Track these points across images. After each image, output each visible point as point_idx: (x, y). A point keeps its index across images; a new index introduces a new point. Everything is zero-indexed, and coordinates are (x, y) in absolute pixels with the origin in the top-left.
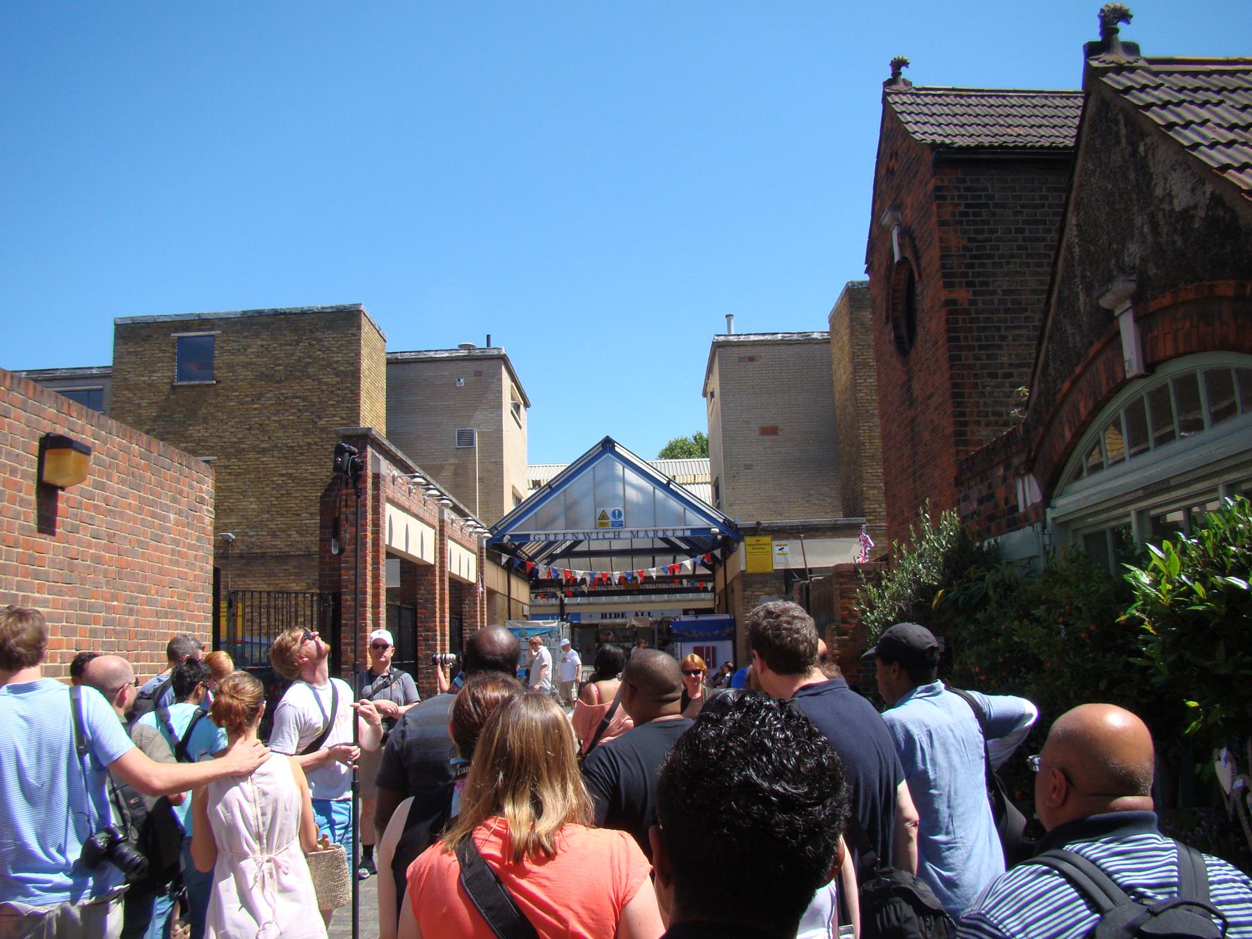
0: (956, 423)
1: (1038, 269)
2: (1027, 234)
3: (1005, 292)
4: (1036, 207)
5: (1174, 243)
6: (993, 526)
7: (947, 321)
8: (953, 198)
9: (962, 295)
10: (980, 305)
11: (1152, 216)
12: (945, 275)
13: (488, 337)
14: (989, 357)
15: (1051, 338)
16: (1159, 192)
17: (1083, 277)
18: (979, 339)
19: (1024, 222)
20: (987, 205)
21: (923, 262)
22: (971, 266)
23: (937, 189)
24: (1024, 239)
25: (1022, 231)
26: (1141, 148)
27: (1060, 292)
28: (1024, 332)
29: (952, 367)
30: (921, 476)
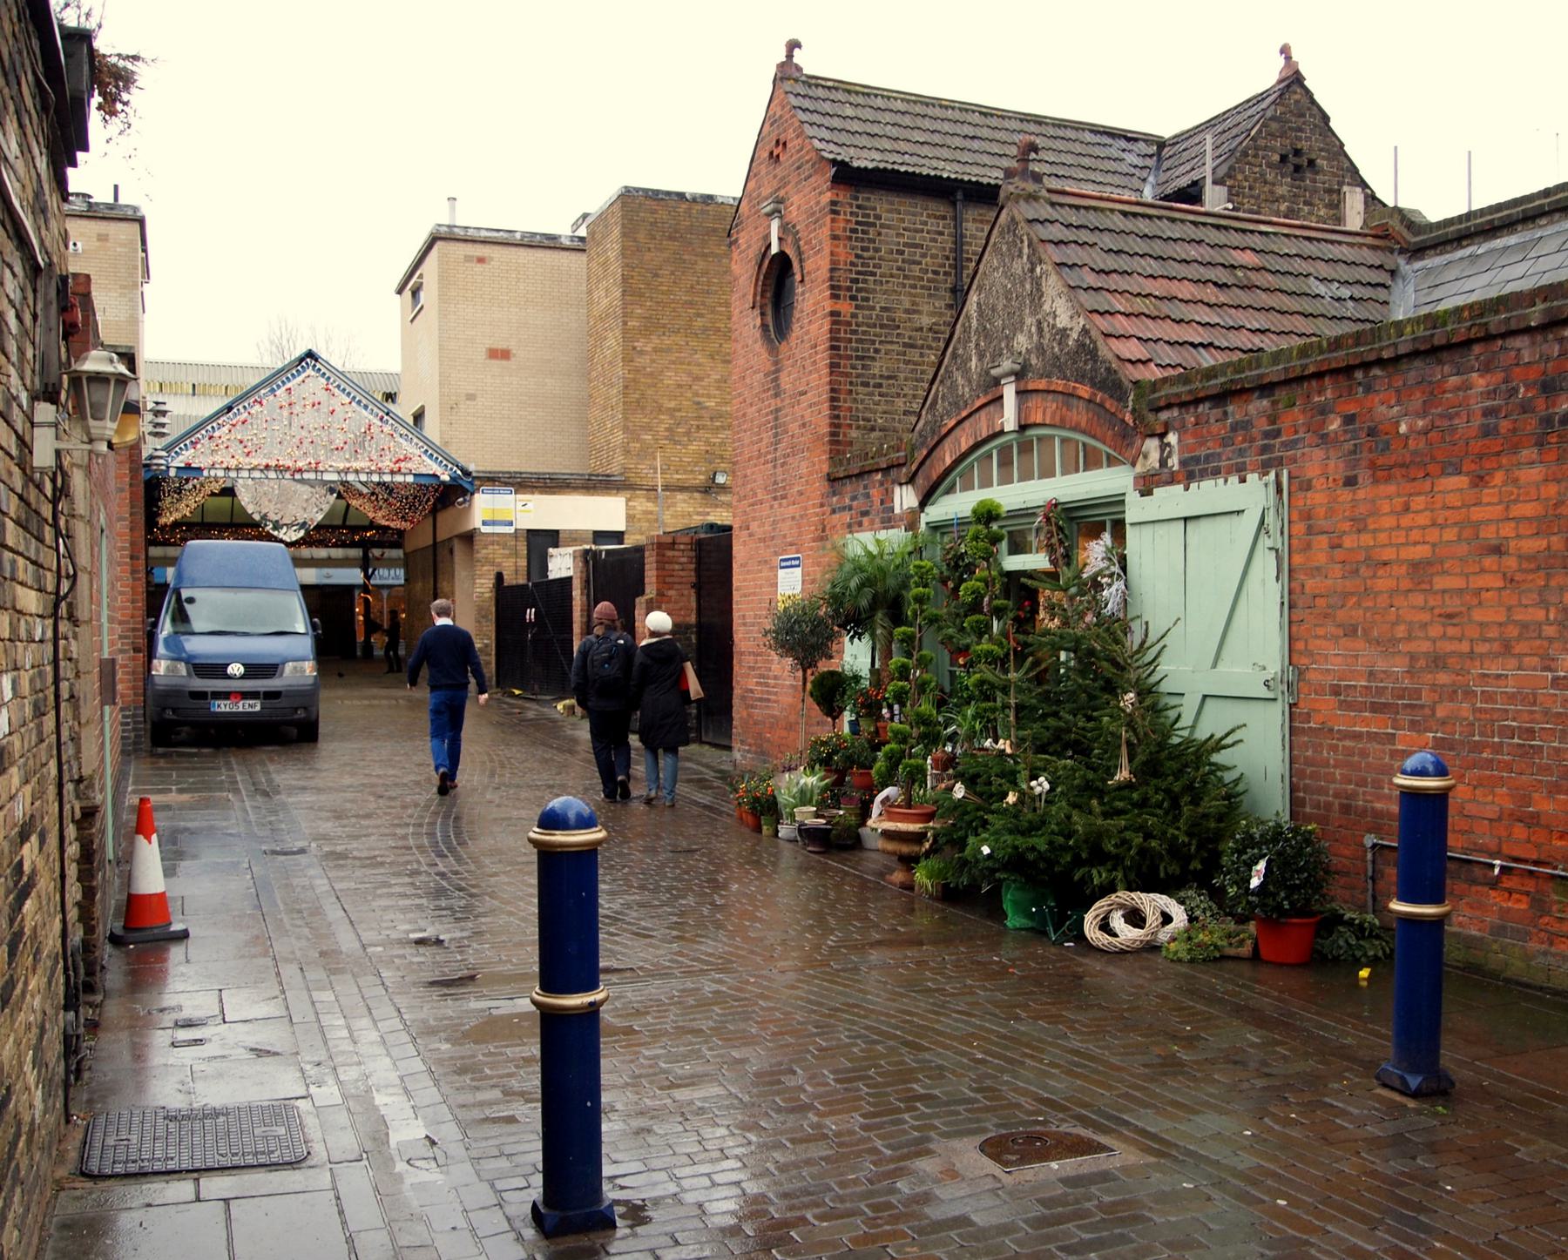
0: (832, 425)
1: (913, 291)
2: (906, 256)
3: (884, 309)
4: (916, 231)
5: (1053, 348)
6: (865, 520)
7: (831, 331)
8: (845, 214)
9: (846, 307)
10: (860, 319)
11: (1039, 323)
12: (832, 287)
13: (116, 187)
14: (864, 367)
15: (942, 382)
16: (1046, 307)
17: (977, 345)
18: (857, 350)
19: (905, 245)
20: (874, 225)
21: (808, 265)
22: (856, 281)
23: (833, 203)
24: (904, 261)
25: (902, 253)
26: (1038, 270)
27: (955, 349)
28: (895, 347)
29: (831, 373)
30: (783, 465)
